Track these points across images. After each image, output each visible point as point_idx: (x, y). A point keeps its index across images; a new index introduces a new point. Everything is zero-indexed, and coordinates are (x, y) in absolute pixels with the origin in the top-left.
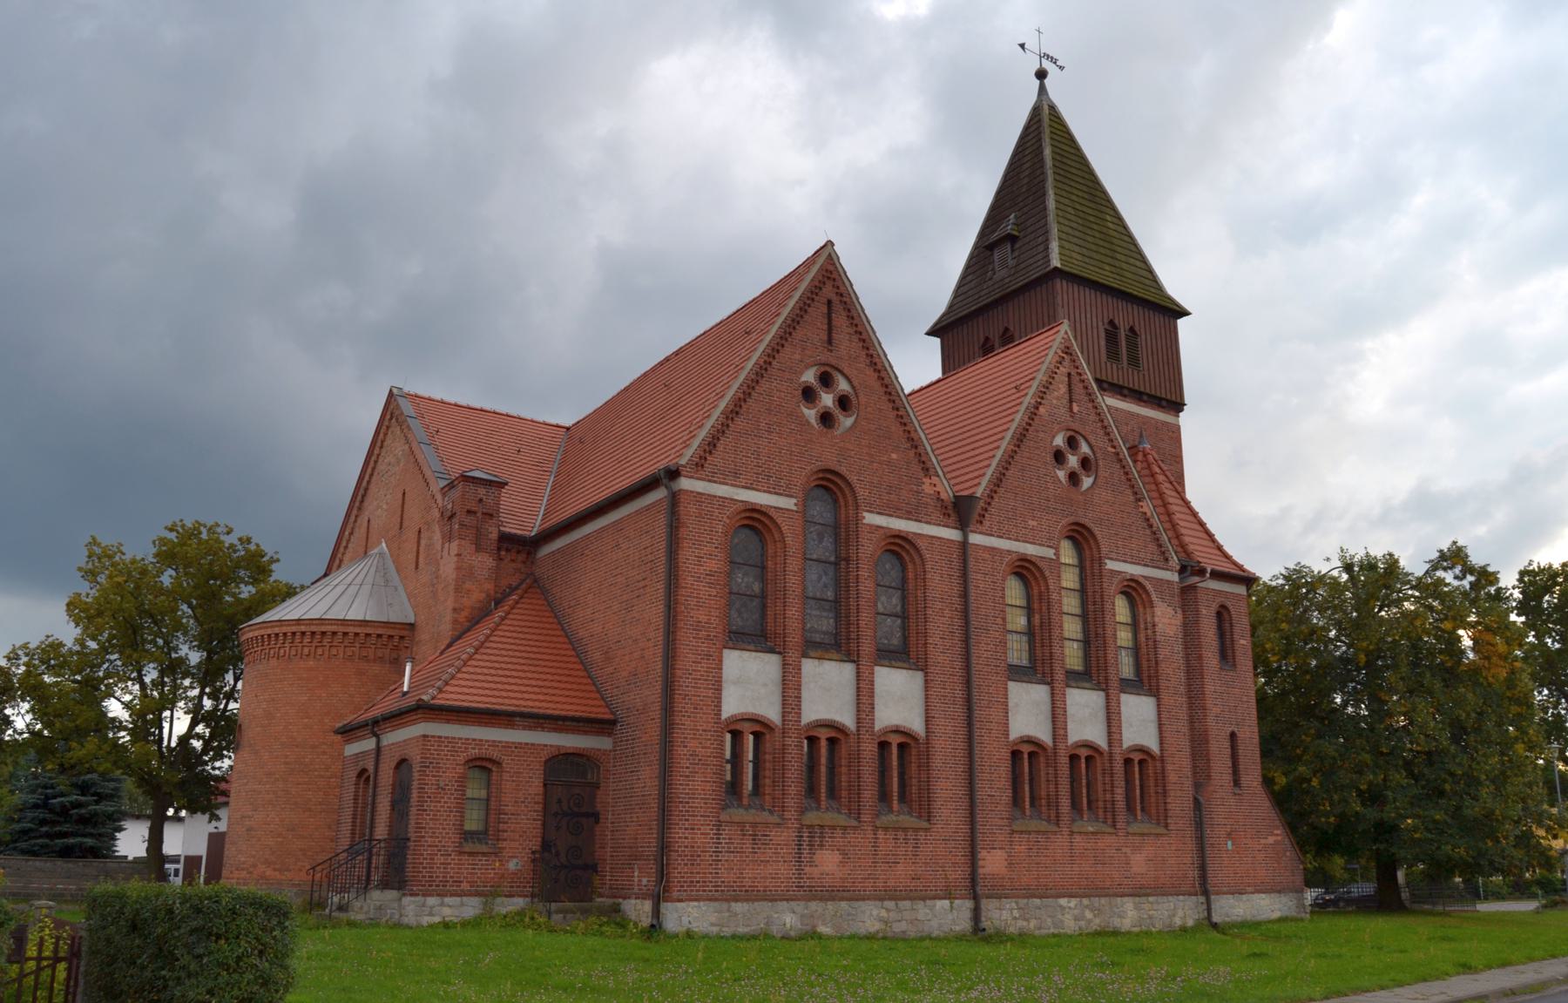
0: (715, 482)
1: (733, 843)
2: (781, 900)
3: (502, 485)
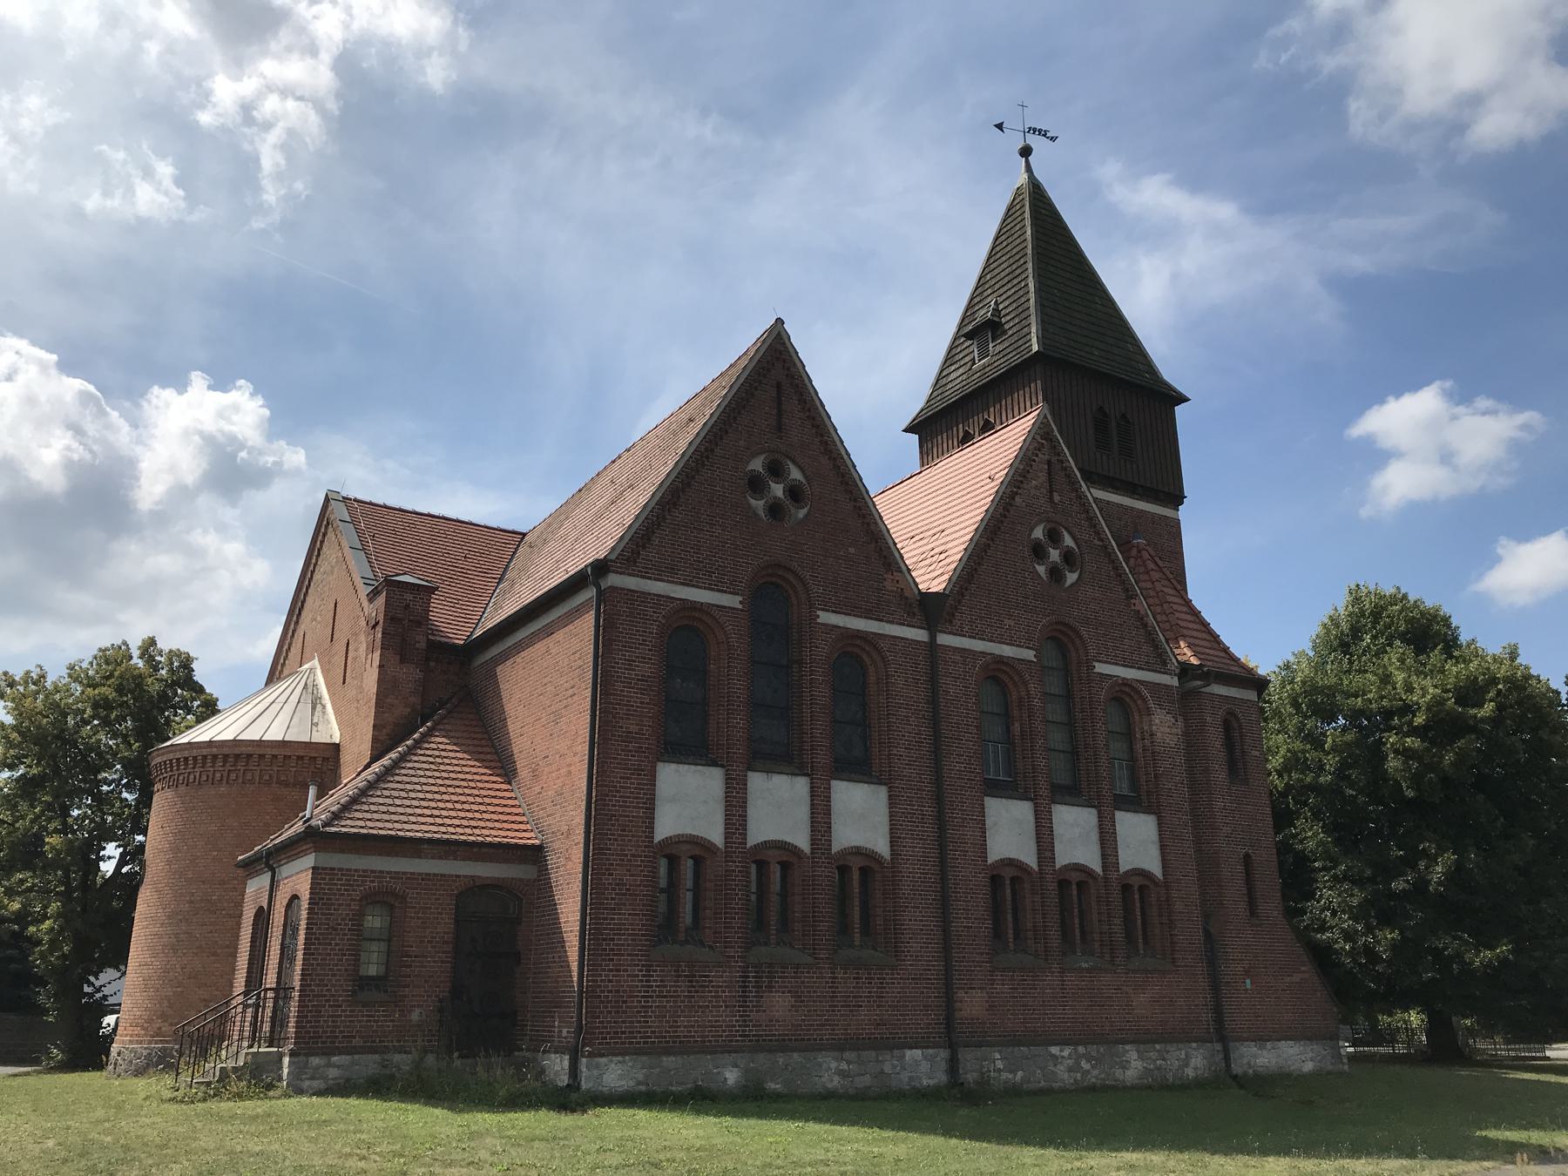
0: (650, 578)
1: (665, 986)
2: (722, 1052)
3: (432, 590)
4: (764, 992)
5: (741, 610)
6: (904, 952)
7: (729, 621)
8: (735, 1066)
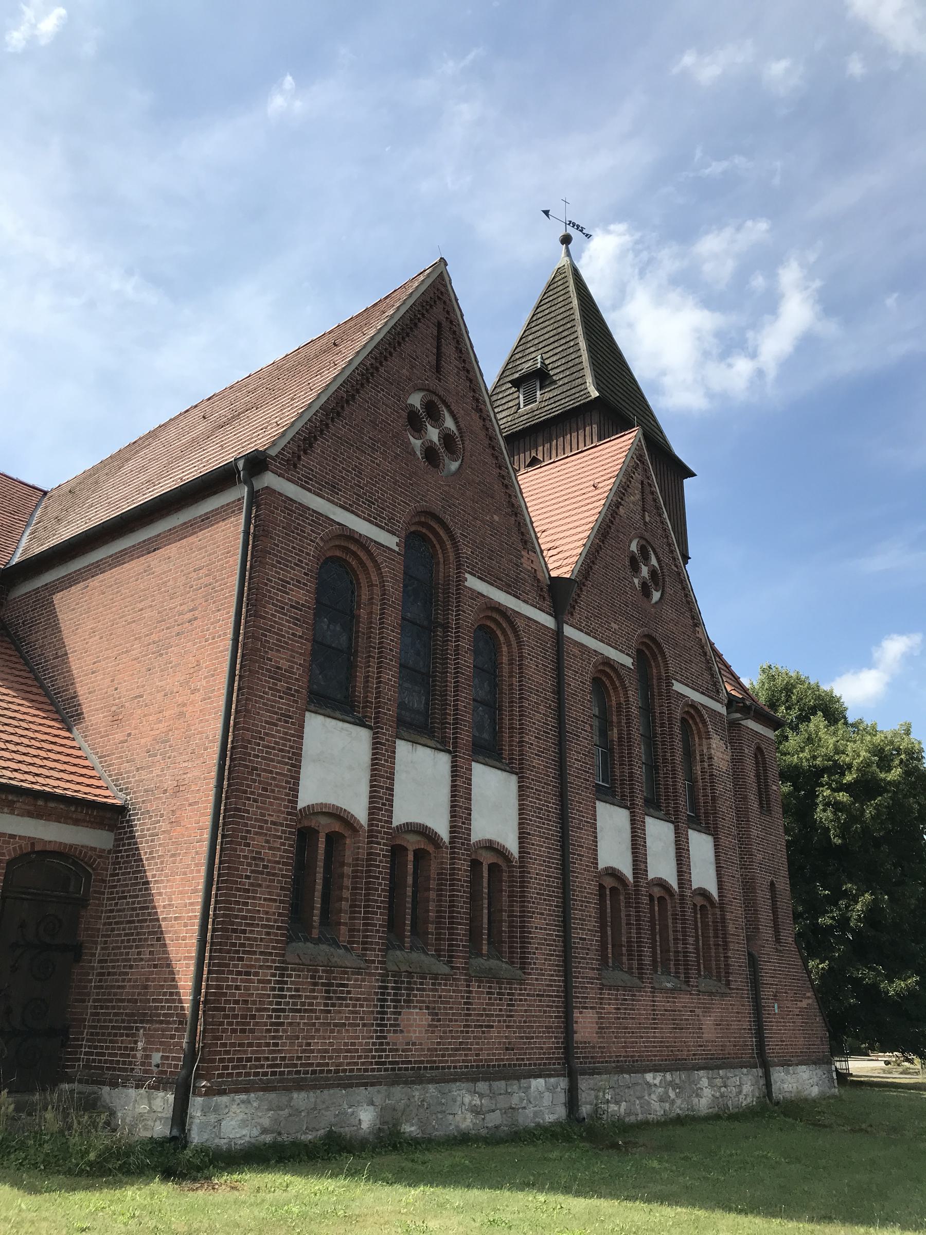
0: (309, 490)
4: (402, 1007)
5: (398, 553)
6: (530, 963)
7: (386, 561)
8: (372, 1103)
